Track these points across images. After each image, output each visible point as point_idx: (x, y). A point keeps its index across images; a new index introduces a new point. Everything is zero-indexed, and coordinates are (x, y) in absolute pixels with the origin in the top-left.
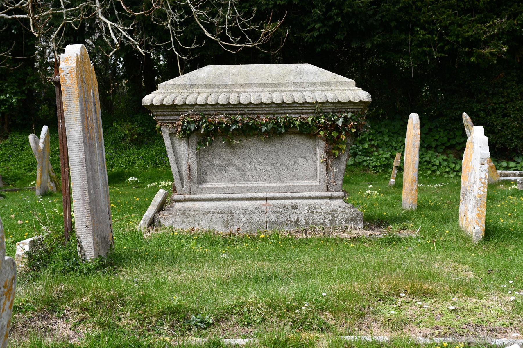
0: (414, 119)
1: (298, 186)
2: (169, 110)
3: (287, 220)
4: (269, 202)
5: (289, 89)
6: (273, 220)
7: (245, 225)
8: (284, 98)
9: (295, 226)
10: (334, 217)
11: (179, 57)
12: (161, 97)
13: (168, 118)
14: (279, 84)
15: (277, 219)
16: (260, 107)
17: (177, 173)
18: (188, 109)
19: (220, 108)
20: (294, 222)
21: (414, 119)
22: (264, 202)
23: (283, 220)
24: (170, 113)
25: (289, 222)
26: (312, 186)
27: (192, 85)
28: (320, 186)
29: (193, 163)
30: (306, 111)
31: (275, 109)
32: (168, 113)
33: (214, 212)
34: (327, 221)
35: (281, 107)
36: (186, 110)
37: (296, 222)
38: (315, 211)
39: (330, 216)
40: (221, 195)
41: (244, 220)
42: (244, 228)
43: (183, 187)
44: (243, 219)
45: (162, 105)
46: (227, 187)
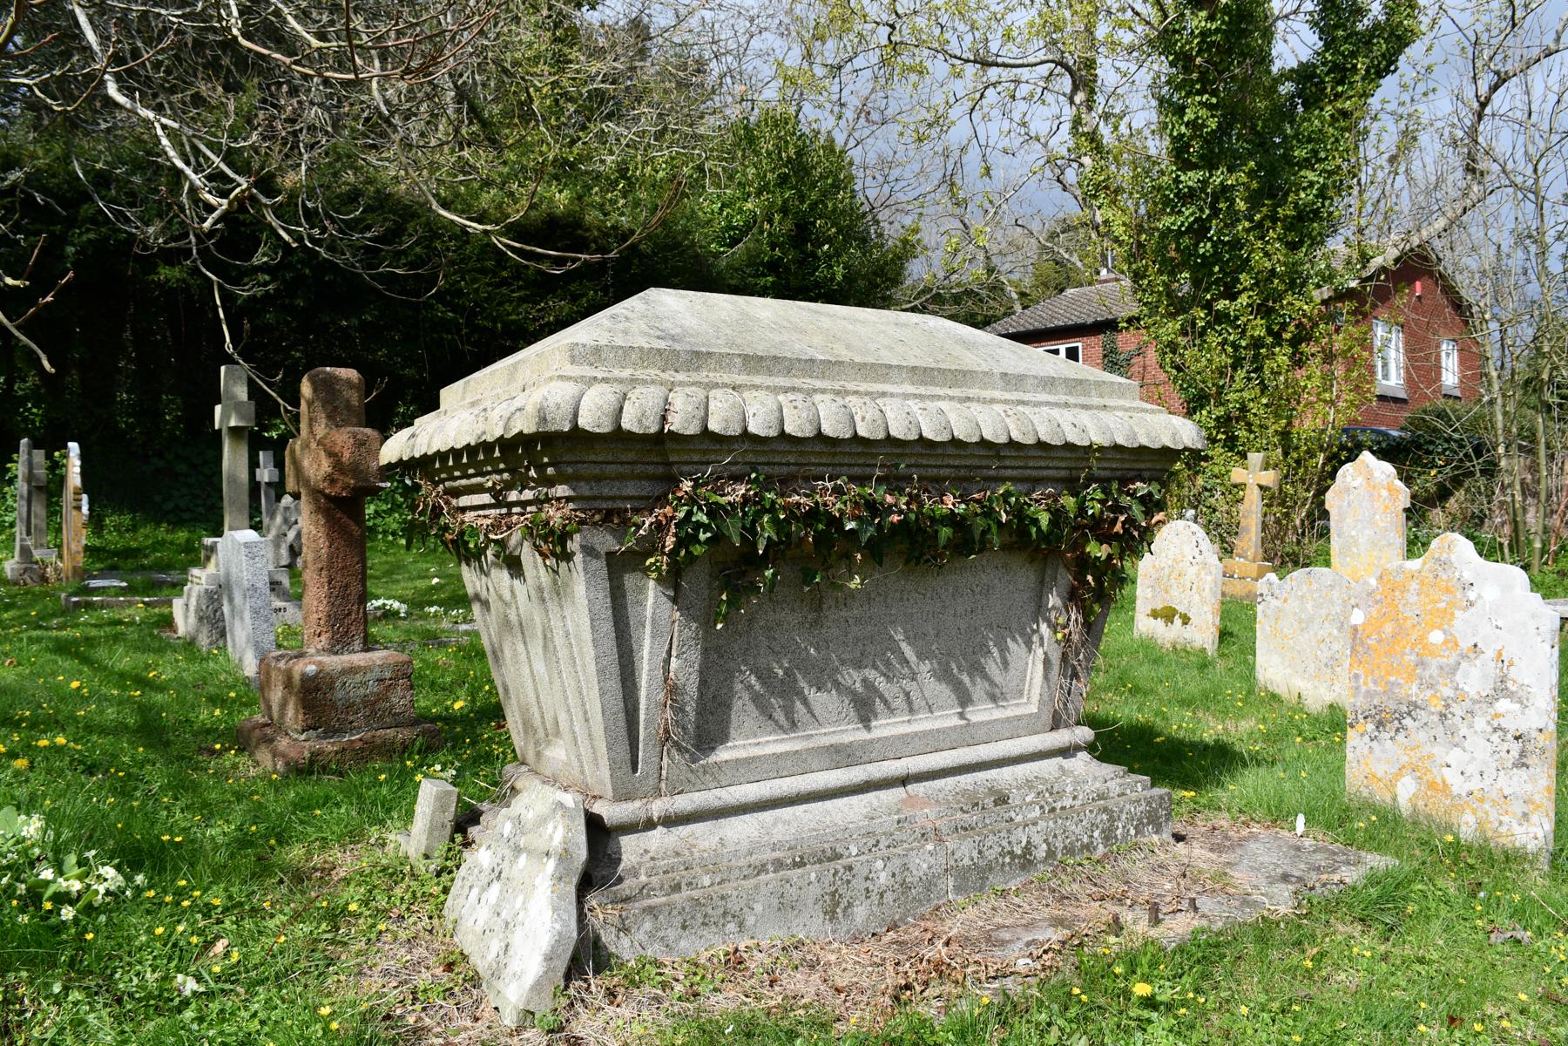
0: (74, 447)
1: (988, 723)
2: (631, 456)
3: (1002, 854)
4: (912, 788)
5: (987, 394)
6: (967, 862)
7: (889, 897)
8: (1012, 427)
9: (1023, 867)
10: (1112, 819)
11: (220, 287)
12: (612, 398)
13: (615, 492)
14: (964, 373)
15: (975, 854)
16: (844, 454)
17: (622, 716)
18: (705, 452)
19: (821, 454)
20: (1019, 857)
21: (74, 447)
22: (899, 792)
23: (991, 854)
24: (626, 469)
25: (1007, 860)
26: (1019, 718)
27: (697, 354)
28: (1037, 716)
29: (686, 670)
30: (1045, 473)
31: (976, 462)
32: (621, 469)
33: (779, 865)
34: (1096, 834)
35: (1000, 458)
36: (696, 458)
37: (1024, 855)
38: (1058, 805)
39: (1105, 817)
40: (769, 784)
41: (883, 878)
42: (885, 909)
43: (635, 770)
44: (883, 875)
45: (619, 436)
46: (787, 753)
